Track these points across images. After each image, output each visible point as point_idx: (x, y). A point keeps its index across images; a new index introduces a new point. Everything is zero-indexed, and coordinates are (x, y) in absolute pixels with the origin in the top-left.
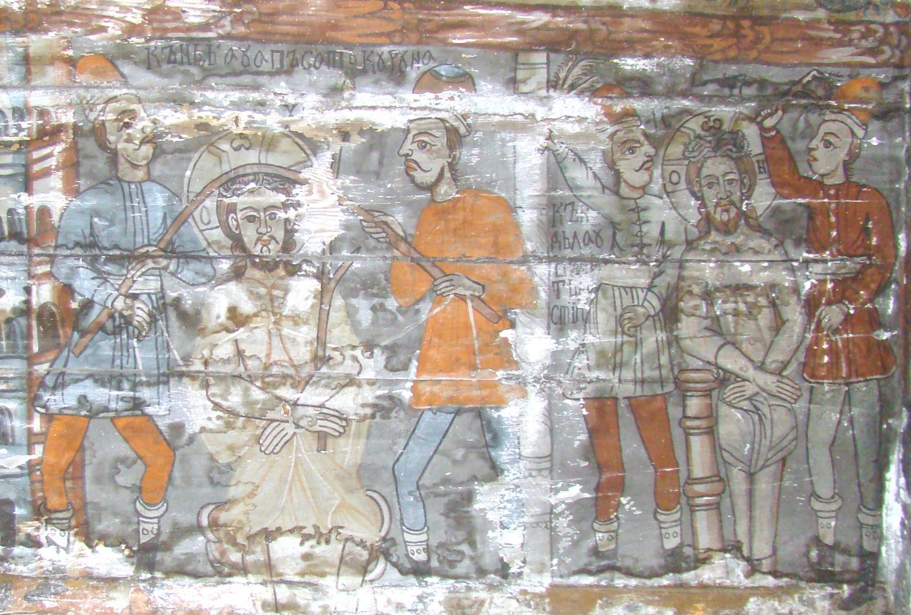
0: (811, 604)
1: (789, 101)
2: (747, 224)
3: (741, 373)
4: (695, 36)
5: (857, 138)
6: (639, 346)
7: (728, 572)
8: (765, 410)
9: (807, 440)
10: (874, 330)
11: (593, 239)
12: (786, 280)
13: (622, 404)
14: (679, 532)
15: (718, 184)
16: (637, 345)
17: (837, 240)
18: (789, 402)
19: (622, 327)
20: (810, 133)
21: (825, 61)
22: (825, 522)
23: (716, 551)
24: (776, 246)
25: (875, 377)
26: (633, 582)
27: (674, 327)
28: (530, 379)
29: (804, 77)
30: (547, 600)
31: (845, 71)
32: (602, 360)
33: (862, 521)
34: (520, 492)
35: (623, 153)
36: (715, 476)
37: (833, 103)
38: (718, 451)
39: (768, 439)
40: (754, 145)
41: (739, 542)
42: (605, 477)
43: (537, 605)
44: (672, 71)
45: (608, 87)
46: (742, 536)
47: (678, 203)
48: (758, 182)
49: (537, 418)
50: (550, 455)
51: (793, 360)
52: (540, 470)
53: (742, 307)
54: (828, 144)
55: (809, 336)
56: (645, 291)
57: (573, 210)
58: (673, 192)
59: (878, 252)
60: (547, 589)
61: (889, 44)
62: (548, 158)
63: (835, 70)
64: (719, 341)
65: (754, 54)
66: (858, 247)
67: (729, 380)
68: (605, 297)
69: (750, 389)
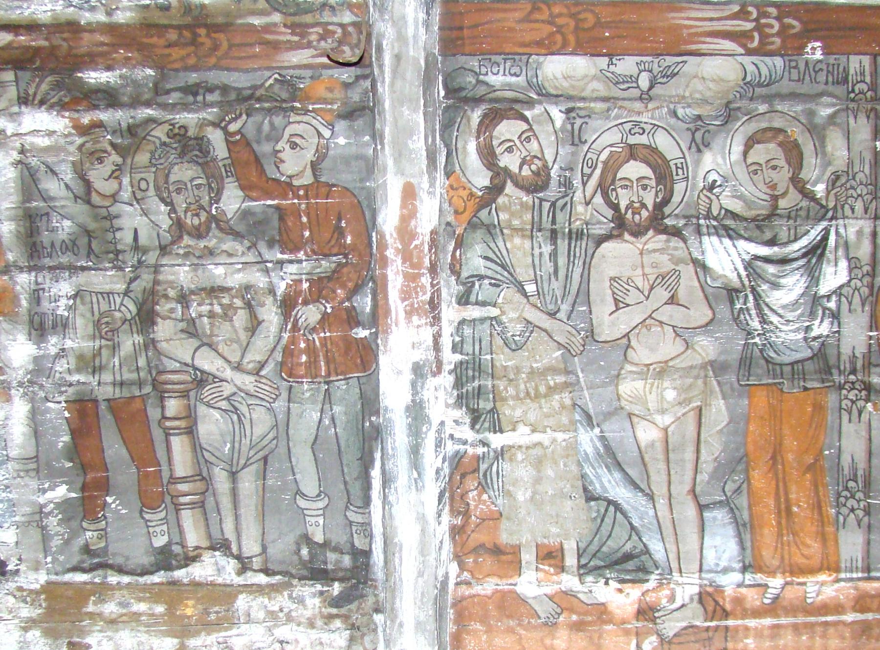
0: (301, 601)
1: (254, 104)
2: (218, 227)
3: (218, 374)
4: (154, 46)
5: (324, 138)
6: (117, 349)
7: (219, 570)
8: (244, 409)
9: (288, 440)
10: (352, 329)
11: (70, 247)
12: (260, 280)
13: (103, 406)
14: (166, 530)
15: (186, 189)
16: (115, 349)
17: (311, 239)
18: (267, 401)
19: (100, 333)
20: (275, 136)
21: (286, 64)
22: (313, 520)
23: (206, 549)
24: (249, 248)
25: (356, 375)
26: (126, 579)
27: (151, 330)
28: (14, 384)
29: (266, 80)
30: (43, 597)
31: (308, 73)
32: (82, 364)
33: (351, 519)
34: (10, 492)
35: (92, 164)
36: (198, 475)
37: (298, 105)
38: (199, 450)
39: (248, 439)
40: (219, 149)
41: (227, 540)
42: (89, 477)
43: (34, 601)
44: (135, 82)
45: (76, 101)
46: (230, 534)
47: (148, 209)
48: (226, 185)
49: (22, 421)
50: (36, 457)
51: (270, 361)
52: (27, 471)
53: (217, 309)
54: (294, 146)
55: (286, 336)
56: (122, 296)
57: (48, 220)
58: (143, 199)
59: (353, 250)
60: (42, 586)
61: (349, 44)
62: (22, 172)
63: (297, 72)
64: (195, 343)
65: (213, 61)
66: (333, 246)
67: (207, 381)
68: (83, 304)
69: (228, 389)
